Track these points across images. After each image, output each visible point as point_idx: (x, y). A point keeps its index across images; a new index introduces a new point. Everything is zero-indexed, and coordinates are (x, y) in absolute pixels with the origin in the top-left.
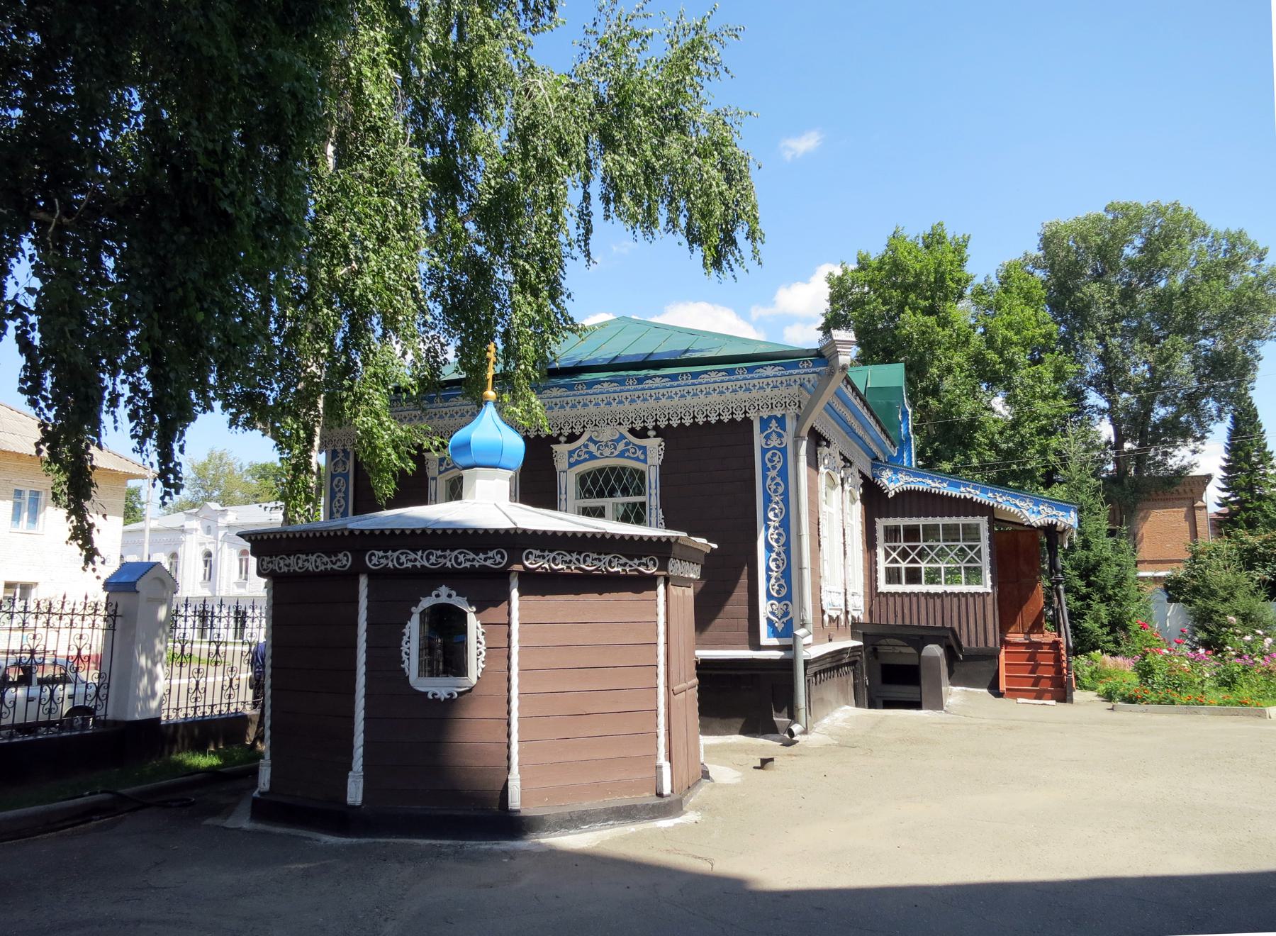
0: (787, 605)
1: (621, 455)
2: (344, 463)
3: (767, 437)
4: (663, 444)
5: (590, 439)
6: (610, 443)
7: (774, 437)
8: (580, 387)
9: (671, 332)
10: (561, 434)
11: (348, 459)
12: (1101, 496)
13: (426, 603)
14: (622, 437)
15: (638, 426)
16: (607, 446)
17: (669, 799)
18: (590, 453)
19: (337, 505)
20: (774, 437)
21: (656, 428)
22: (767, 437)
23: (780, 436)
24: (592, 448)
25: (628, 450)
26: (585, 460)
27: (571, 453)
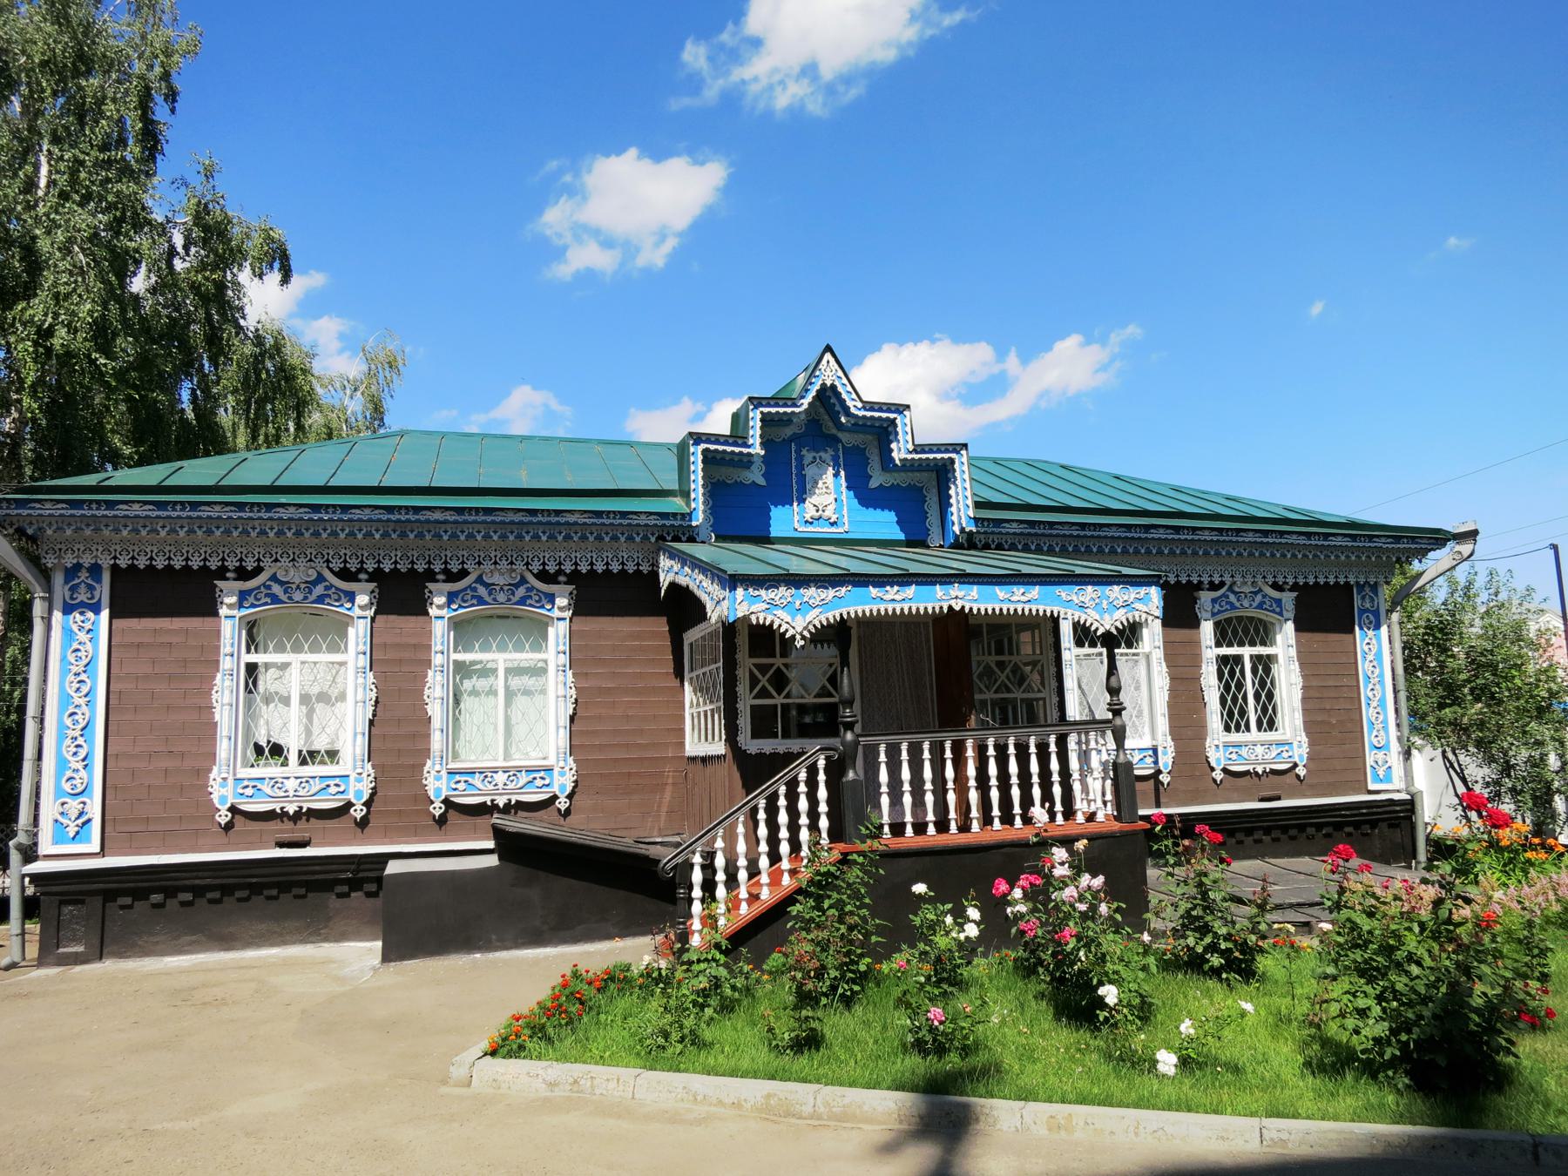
0: (84, 803)
1: (1260, 606)
2: (91, 588)
3: (73, 589)
4: (377, 590)
5: (274, 578)
6: (303, 586)
7: (1367, 600)
8: (1186, 532)
10: (1285, 583)
11: (99, 581)
12: (233, 348)
13: (975, 677)
14: (320, 578)
15: (552, 568)
16: (298, 587)
17: (931, 839)
18: (1231, 604)
19: (1367, 621)
20: (1367, 600)
21: (446, 571)
22: (73, 589)
23: (91, 588)
24: (277, 589)
25: (530, 597)
26: (1227, 610)
27: (1214, 601)
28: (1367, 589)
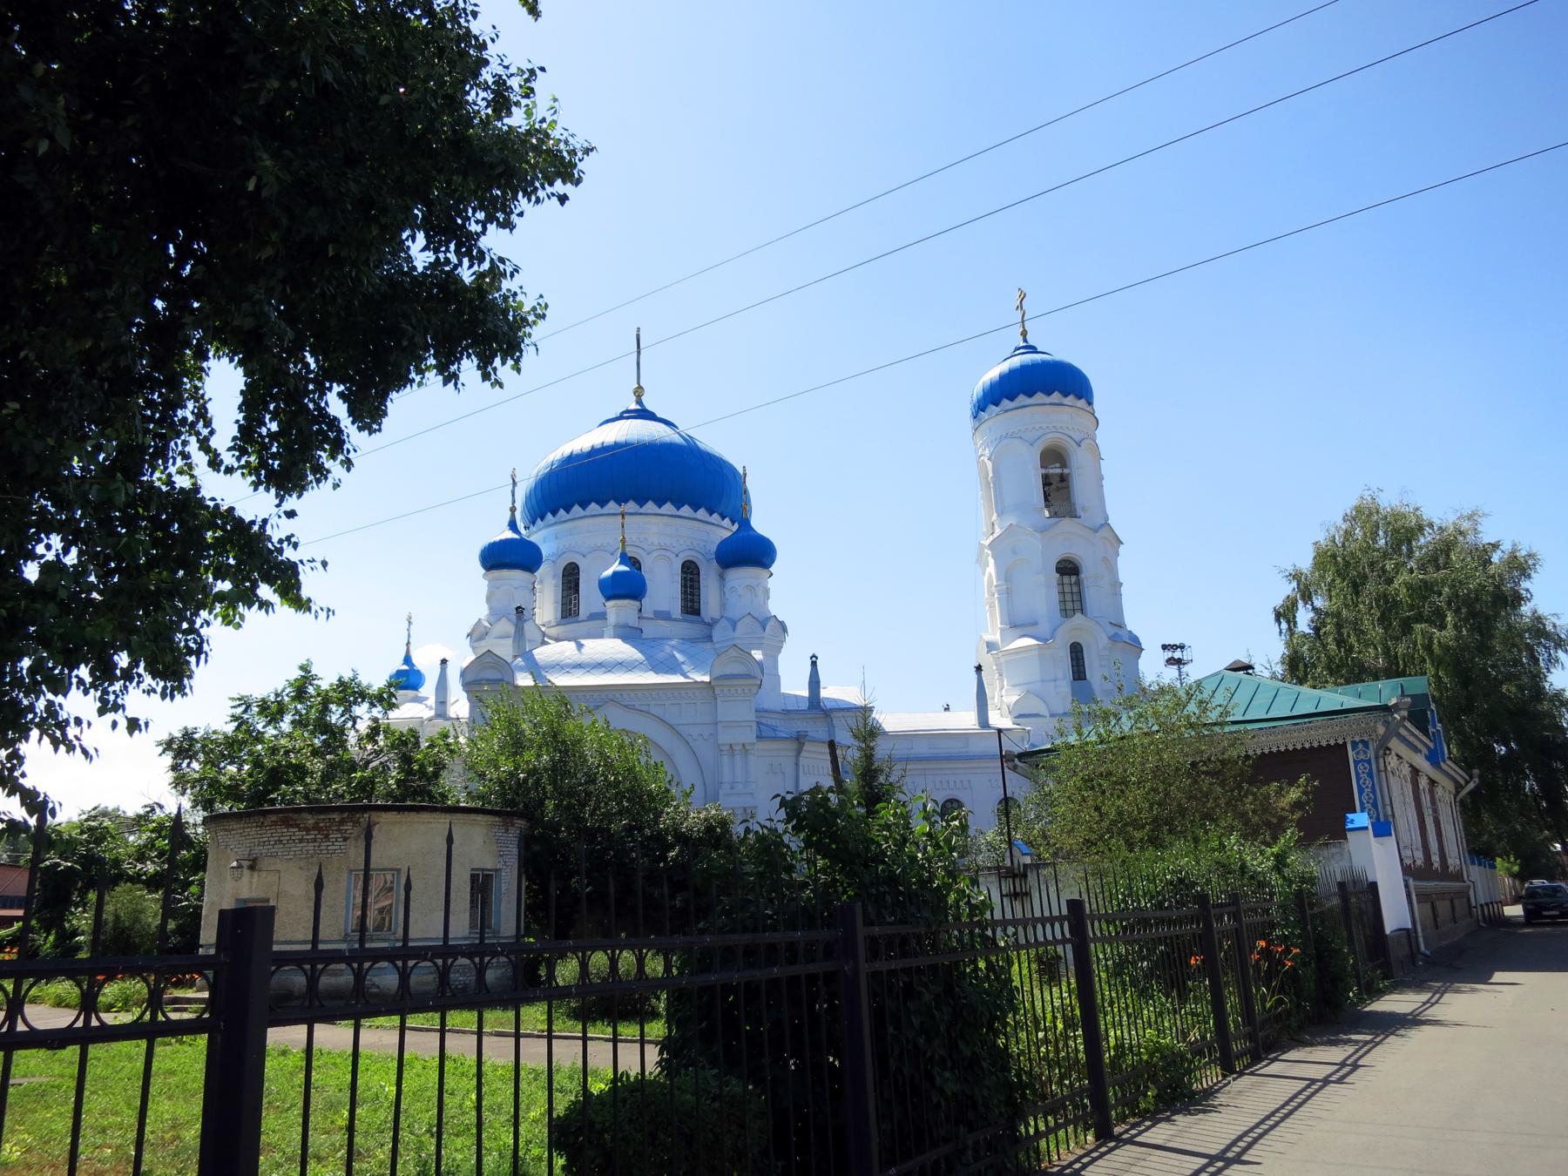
9: (1220, 677)
22: (1357, 753)
28: (1360, 746)
